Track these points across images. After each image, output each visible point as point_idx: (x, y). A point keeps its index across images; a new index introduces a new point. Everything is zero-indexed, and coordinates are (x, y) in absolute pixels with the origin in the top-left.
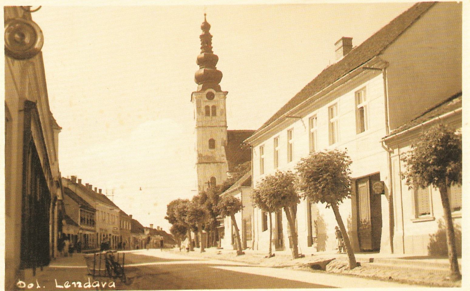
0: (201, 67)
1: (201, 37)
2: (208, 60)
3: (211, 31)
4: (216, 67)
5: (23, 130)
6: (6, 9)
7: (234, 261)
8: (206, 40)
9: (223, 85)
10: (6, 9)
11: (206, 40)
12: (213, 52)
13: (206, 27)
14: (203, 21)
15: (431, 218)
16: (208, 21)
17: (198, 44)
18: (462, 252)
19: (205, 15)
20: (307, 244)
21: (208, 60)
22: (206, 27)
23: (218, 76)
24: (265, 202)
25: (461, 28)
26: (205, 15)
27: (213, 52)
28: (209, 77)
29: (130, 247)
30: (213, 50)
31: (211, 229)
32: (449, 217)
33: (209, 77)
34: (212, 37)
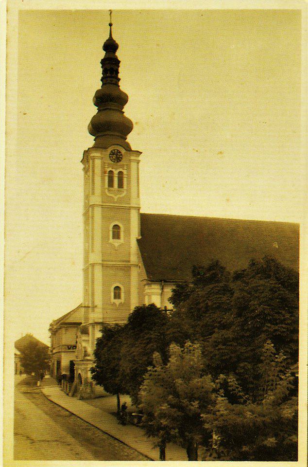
0: (102, 109)
1: (103, 62)
2: (110, 98)
3: (119, 54)
6: (297, 461)
8: (111, 66)
10: (297, 461)
11: (111, 66)
12: (124, 113)
13: (111, 47)
14: (107, 37)
15: (101, 318)
17: (98, 72)
18: (299, 382)
19: (111, 25)
21: (110, 98)
22: (111, 47)
23: (126, 127)
24: (92, 391)
26: (111, 25)
27: (124, 113)
28: (110, 124)
29: (258, 315)
30: (120, 83)
33: (110, 124)
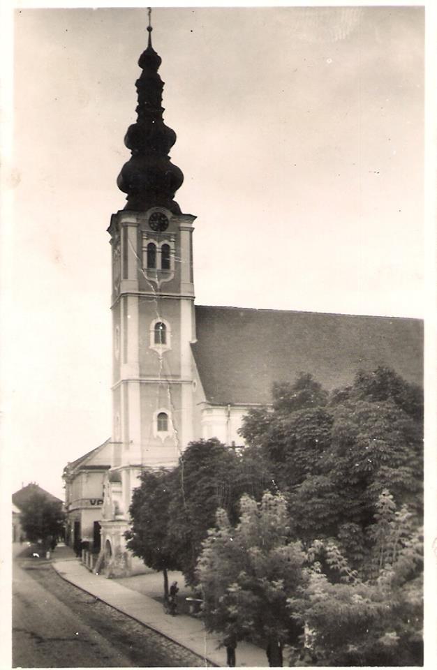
2: (150, 140)
4: (169, 155)
5: (201, 625)
7: (148, 298)
8: (150, 89)
9: (184, 198)
11: (150, 89)
16: (155, 48)
19: (150, 29)
20: (426, 9)
21: (150, 140)
25: (356, 317)
26: (150, 29)
27: (170, 158)
28: (150, 179)
30: (164, 115)
31: (143, 492)
32: (339, 401)
33: (150, 179)
34: (164, 83)
